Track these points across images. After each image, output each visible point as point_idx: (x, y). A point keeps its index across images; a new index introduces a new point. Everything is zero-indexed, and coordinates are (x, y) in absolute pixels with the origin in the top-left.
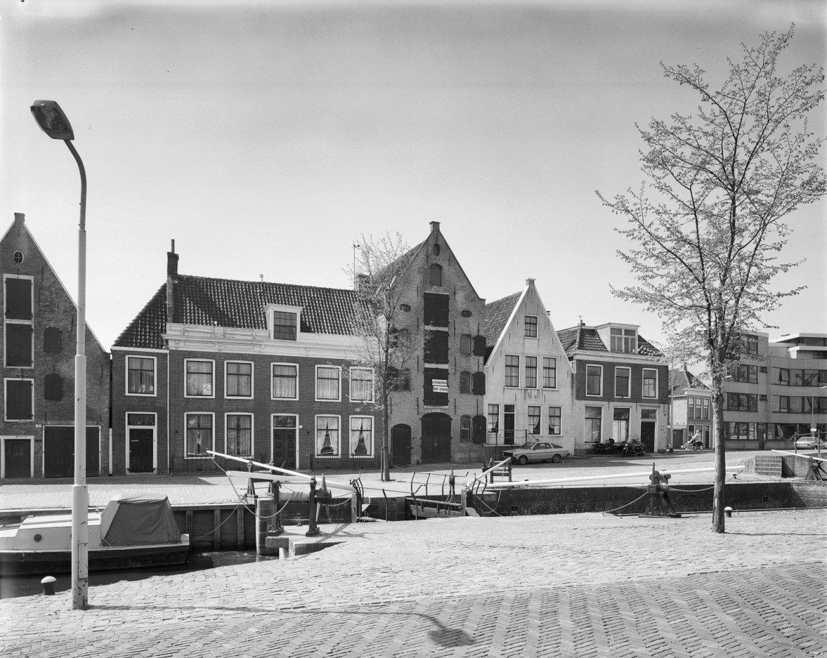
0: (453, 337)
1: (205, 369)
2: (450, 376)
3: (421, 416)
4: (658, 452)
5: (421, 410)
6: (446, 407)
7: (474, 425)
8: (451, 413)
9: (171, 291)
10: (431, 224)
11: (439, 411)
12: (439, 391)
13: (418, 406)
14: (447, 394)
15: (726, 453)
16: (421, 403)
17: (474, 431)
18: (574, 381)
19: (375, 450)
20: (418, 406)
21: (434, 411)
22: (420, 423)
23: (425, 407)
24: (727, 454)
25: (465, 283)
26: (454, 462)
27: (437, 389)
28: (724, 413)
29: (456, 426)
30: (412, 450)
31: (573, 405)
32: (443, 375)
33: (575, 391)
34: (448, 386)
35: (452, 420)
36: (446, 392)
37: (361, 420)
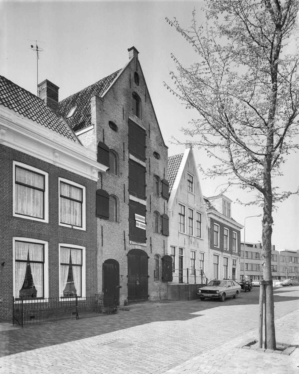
0: (149, 175)
1: (76, 195)
2: (147, 213)
3: (127, 252)
4: (241, 292)
5: (127, 245)
6: (144, 245)
7: (163, 264)
8: (148, 252)
9: (269, 296)
10: (129, 50)
11: (140, 248)
12: (139, 227)
13: (125, 240)
14: (145, 230)
15: (275, 303)
16: (127, 237)
17: (163, 270)
18: (209, 234)
19: (87, 290)
20: (125, 240)
21: (137, 247)
22: (126, 258)
23: (131, 242)
24: (276, 304)
25: (145, 86)
26: (151, 301)
27: (138, 225)
28: (272, 273)
29: (152, 264)
30: (121, 289)
31: (209, 252)
32: (142, 210)
33: (210, 242)
34: (146, 223)
35: (149, 258)
36: (145, 229)
37: (69, 250)
